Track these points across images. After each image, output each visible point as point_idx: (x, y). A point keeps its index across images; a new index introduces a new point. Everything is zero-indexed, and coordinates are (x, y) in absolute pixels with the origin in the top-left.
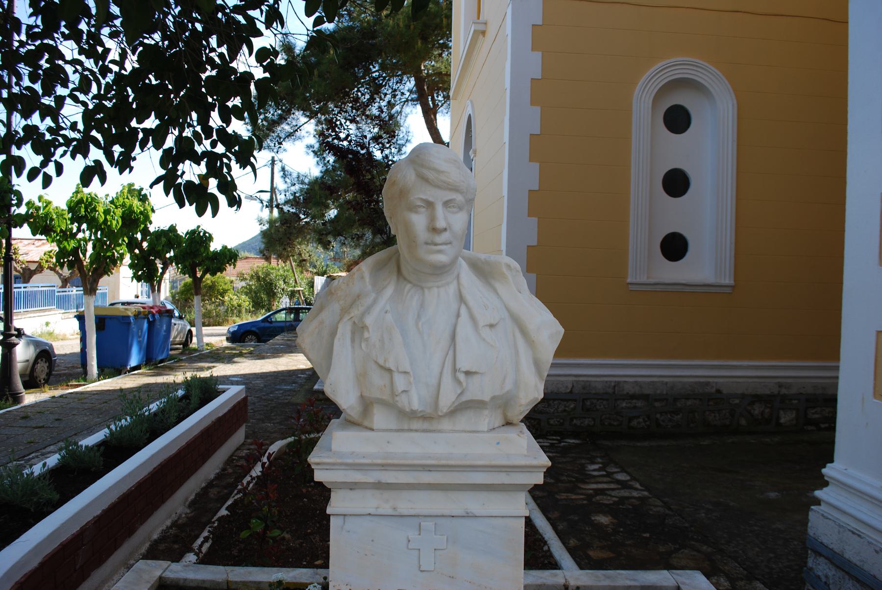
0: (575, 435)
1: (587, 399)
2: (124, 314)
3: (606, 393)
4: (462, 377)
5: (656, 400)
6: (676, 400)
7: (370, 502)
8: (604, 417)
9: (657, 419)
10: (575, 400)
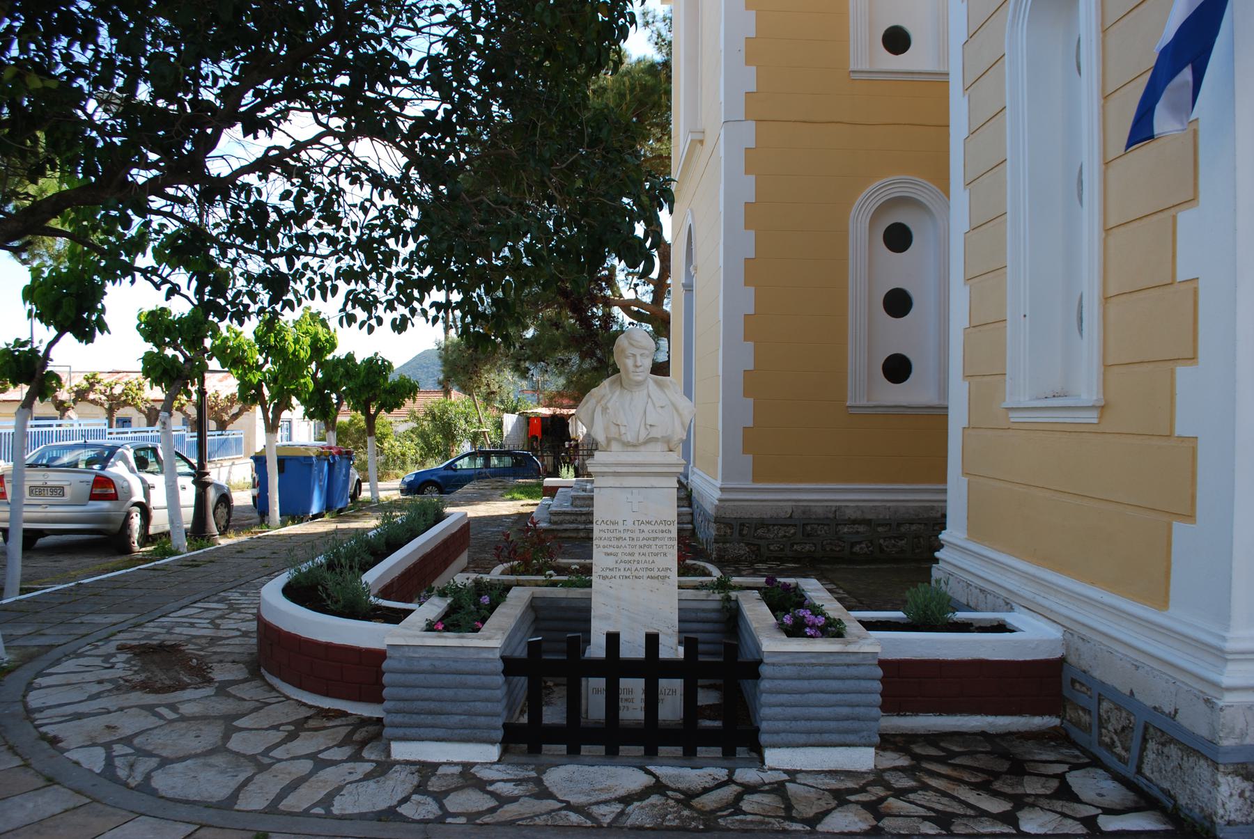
0: (794, 560)
1: (807, 524)
2: (306, 455)
3: (827, 518)
4: (648, 427)
5: (879, 525)
6: (899, 525)
7: (611, 481)
8: (825, 543)
9: (881, 544)
10: (795, 526)
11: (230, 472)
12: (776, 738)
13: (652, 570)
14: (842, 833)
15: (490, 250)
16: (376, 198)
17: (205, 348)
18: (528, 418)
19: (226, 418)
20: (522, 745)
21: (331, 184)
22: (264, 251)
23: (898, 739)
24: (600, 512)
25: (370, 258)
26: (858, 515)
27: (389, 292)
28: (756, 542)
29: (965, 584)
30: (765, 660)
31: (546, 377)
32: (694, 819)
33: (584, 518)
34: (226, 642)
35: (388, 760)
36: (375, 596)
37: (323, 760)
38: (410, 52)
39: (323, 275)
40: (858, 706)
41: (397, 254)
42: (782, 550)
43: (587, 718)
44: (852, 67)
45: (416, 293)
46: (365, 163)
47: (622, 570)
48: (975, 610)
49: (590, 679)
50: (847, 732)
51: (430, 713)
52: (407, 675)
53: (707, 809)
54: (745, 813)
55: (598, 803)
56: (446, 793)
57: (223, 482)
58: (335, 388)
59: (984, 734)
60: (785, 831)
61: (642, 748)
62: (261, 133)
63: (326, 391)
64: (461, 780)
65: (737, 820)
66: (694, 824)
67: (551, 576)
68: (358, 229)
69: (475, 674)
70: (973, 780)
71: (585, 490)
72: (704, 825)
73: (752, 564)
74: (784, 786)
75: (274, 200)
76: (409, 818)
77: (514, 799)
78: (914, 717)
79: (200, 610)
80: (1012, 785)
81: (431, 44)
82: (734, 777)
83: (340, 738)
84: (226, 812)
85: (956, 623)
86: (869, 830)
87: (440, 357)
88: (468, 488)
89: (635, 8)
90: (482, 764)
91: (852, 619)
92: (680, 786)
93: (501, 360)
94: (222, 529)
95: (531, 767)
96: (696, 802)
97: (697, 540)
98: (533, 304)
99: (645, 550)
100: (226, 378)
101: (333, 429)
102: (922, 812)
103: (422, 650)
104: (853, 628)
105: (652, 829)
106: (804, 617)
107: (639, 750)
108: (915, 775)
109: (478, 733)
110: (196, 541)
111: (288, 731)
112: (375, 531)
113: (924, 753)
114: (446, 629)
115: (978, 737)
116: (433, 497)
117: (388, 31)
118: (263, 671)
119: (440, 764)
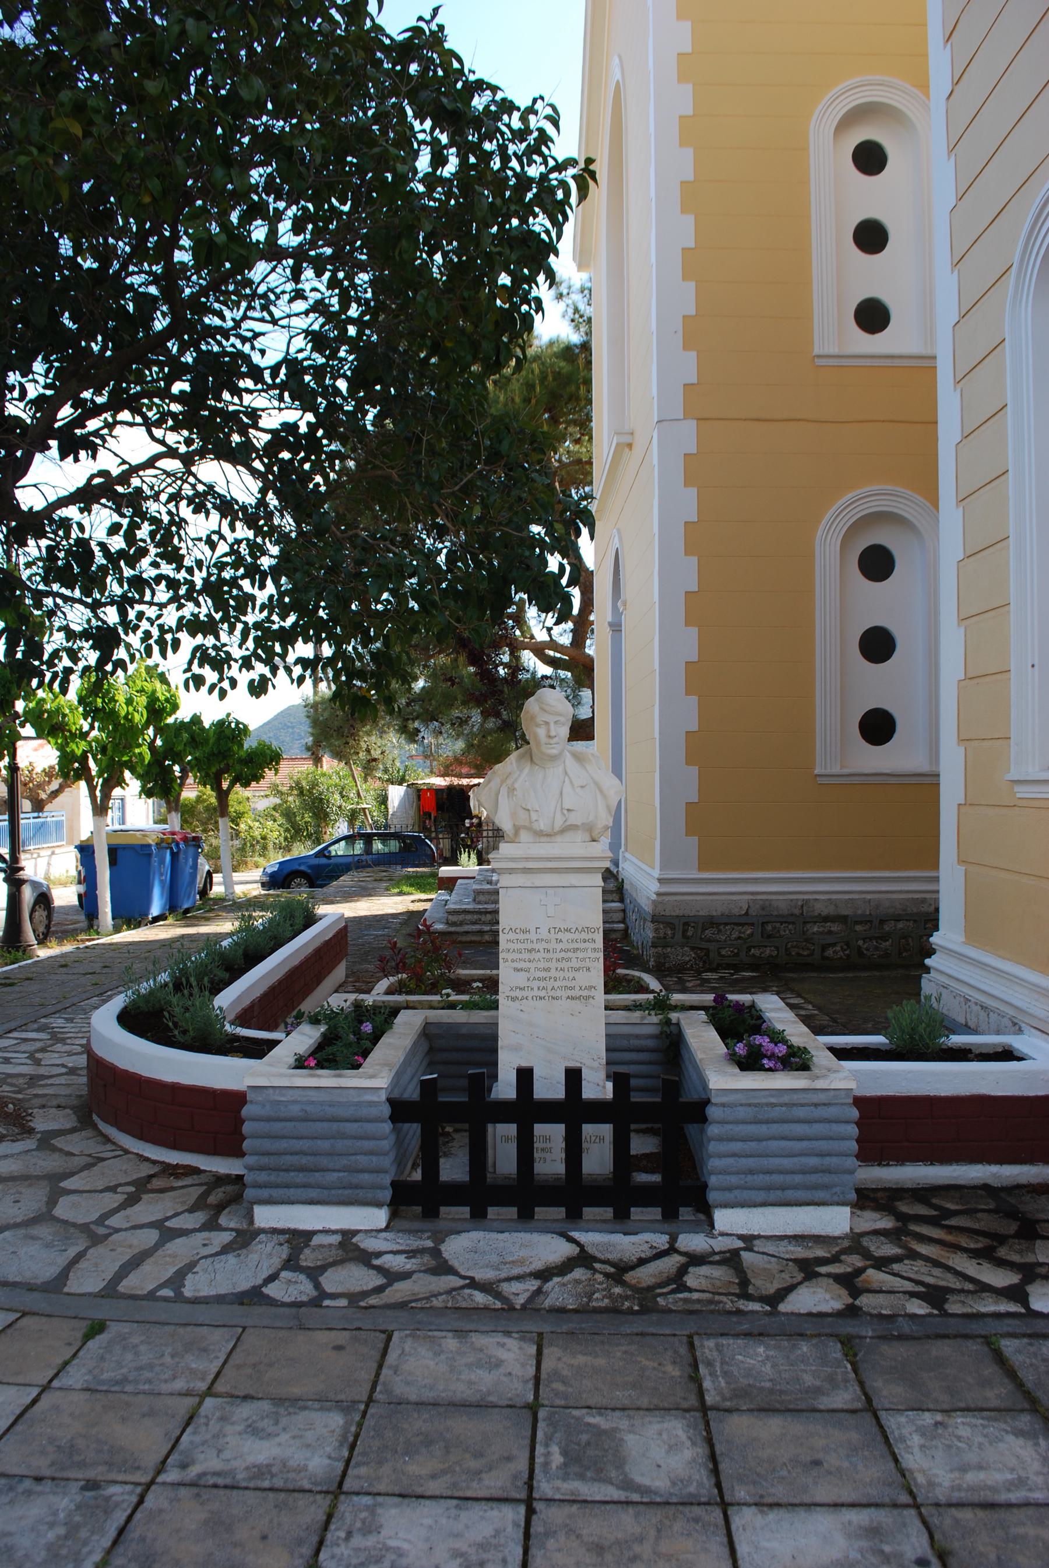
0: (753, 967)
1: (767, 923)
4: (565, 812)
5: (857, 923)
6: (882, 922)
8: (789, 945)
9: (859, 947)
10: (753, 924)
11: (49, 864)
12: (728, 1196)
13: (572, 988)
14: (810, 1314)
15: (368, 596)
16: (225, 530)
17: (16, 713)
18: (419, 791)
19: (43, 796)
20: (415, 1208)
21: (170, 513)
22: (89, 600)
23: (879, 1195)
24: (506, 920)
25: (220, 604)
26: (830, 910)
27: (244, 647)
28: (704, 945)
29: (962, 999)
30: (713, 1100)
31: (441, 740)
32: (627, 1298)
33: (489, 917)
34: (49, 1081)
35: (251, 1228)
36: (232, 1023)
37: (170, 1229)
38: (263, 352)
39: (161, 627)
40: (829, 1155)
41: (253, 598)
42: (737, 955)
43: (495, 1172)
44: (817, 351)
45: (278, 648)
46: (211, 487)
47: (536, 989)
48: (975, 1032)
49: (498, 1125)
50: (815, 1187)
51: (302, 1169)
52: (272, 1123)
53: (644, 1285)
54: (690, 1290)
55: (509, 1279)
56: (323, 1269)
57: (40, 878)
58: (178, 758)
59: (986, 1187)
60: (739, 1312)
61: (563, 1209)
62: (82, 454)
63: (167, 763)
64: (340, 1252)
65: (681, 1299)
66: (627, 1304)
67: (448, 995)
68: (204, 569)
69: (356, 1121)
70: (972, 1246)
71: (490, 882)
72: (640, 1305)
73: (699, 973)
74: (739, 1255)
75: (100, 534)
76: (278, 1301)
77: (406, 1276)
78: (899, 1168)
79: (16, 1042)
80: (1020, 1252)
81: (291, 338)
82: (677, 1245)
83: (192, 1200)
84: (53, 1296)
85: (951, 1050)
86: (843, 1310)
87: (308, 717)
88: (345, 880)
89: (298, 1562)
90: (366, 1231)
91: (818, 1046)
92: (610, 1257)
93: (384, 718)
94: (41, 936)
95: (427, 1235)
96: (629, 1277)
97: (631, 943)
98: (422, 649)
99: (564, 965)
100: (42, 746)
101: (176, 810)
102: (909, 1286)
103: (291, 1092)
104: (822, 1058)
105: (576, 1311)
106: (761, 1045)
107: (560, 1212)
108: (901, 1240)
109: (361, 1194)
110: (10, 952)
111: (127, 1193)
112: (230, 940)
113: (911, 1212)
114: (320, 1065)
115: (979, 1192)
116: (301, 893)
117: (237, 324)
118: (95, 1117)
119: (314, 1233)
